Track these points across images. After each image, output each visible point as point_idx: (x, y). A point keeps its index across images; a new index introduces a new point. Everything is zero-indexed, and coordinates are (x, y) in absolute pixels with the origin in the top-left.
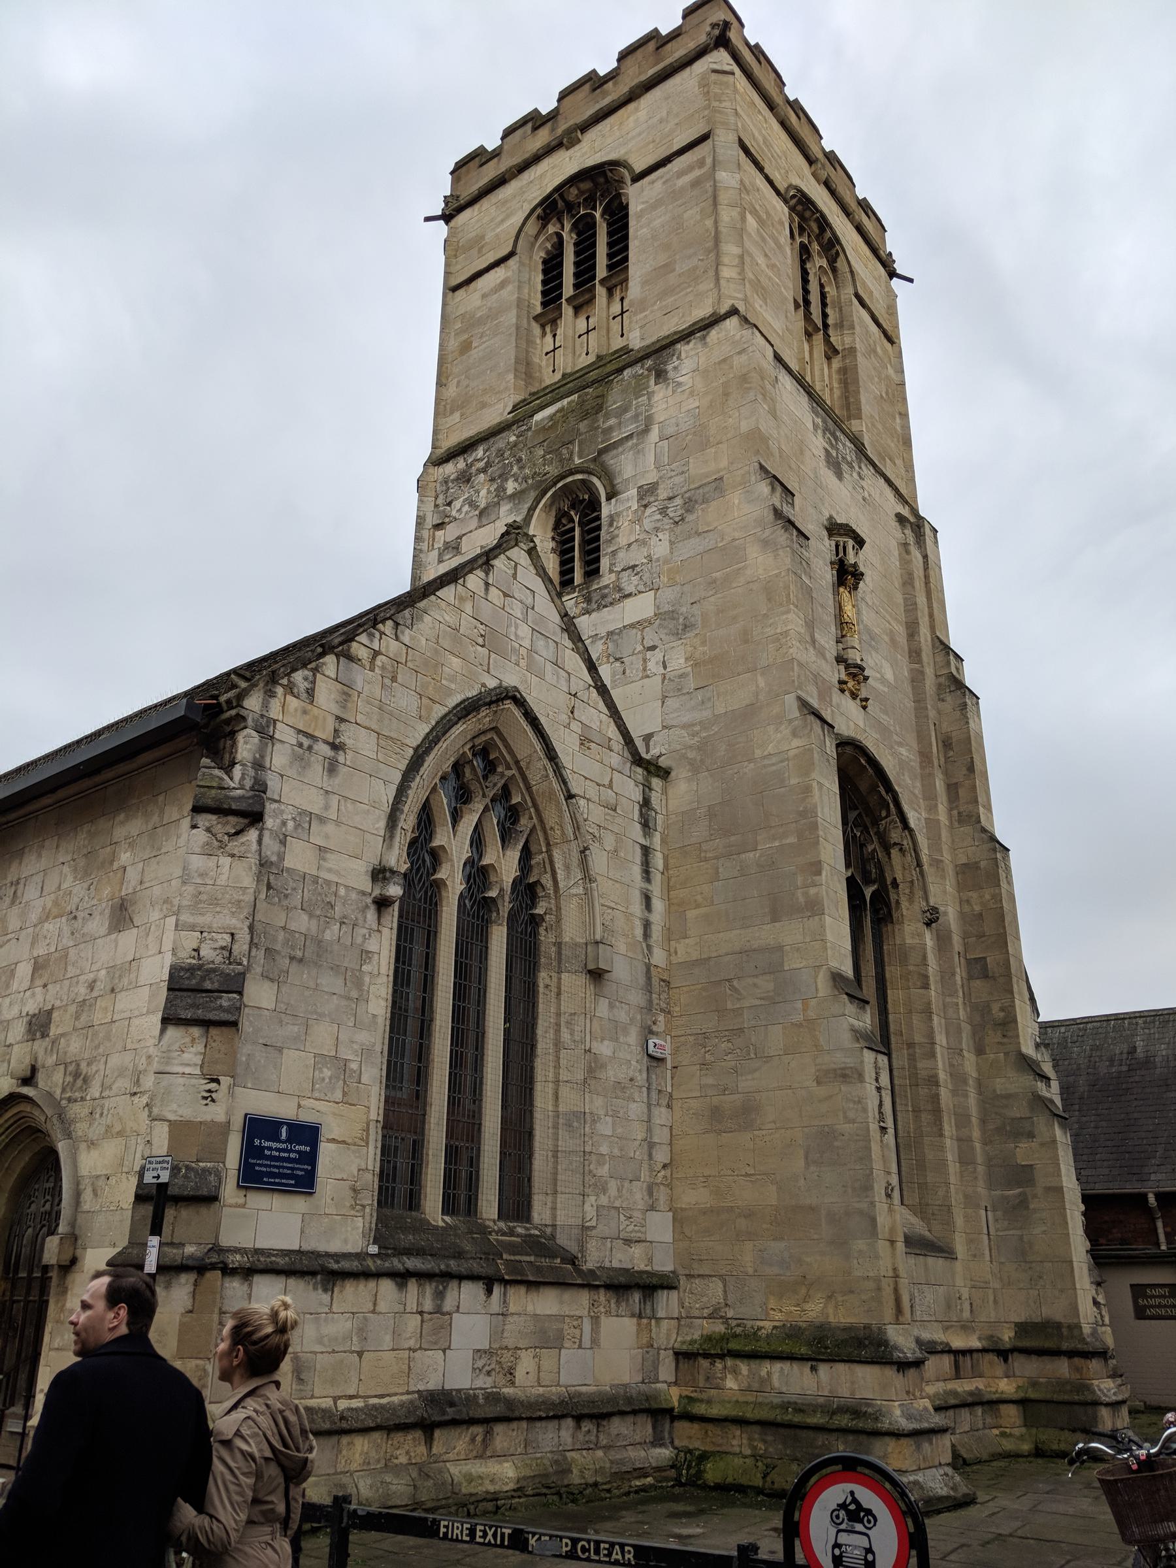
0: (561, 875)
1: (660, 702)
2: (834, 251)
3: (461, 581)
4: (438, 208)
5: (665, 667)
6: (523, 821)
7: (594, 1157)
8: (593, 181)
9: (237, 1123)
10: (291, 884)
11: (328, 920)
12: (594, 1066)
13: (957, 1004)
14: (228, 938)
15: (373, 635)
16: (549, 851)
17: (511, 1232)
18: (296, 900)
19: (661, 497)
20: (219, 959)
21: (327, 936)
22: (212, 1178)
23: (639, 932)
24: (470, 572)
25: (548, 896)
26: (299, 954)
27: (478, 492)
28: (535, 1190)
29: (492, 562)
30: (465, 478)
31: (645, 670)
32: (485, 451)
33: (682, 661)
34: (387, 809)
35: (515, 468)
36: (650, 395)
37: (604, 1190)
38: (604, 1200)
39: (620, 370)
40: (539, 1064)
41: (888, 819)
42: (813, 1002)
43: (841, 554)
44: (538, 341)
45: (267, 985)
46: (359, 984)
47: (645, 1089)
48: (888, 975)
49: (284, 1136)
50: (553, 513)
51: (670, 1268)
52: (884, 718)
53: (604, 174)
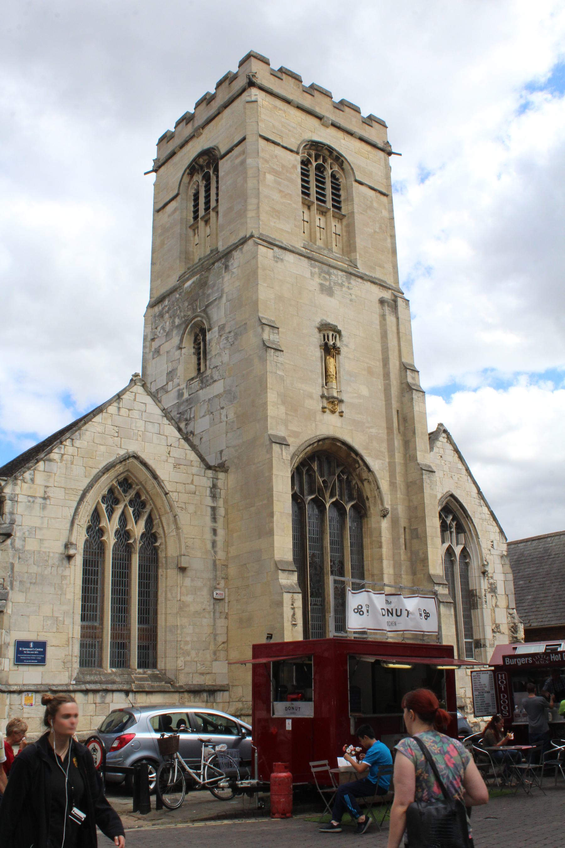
0: (166, 528)
1: (225, 435)
2: (340, 161)
3: (105, 411)
4: (150, 166)
5: (227, 418)
6: (148, 506)
7: (182, 643)
9: (12, 643)
10: (29, 556)
13: (400, 553)
14: (2, 580)
15: (61, 448)
16: (160, 518)
17: (144, 673)
21: (46, 573)
23: (209, 546)
24: (110, 405)
25: (161, 537)
26: (34, 581)
29: (122, 397)
30: (161, 315)
33: (233, 414)
34: (71, 518)
35: (178, 312)
36: (223, 278)
38: (188, 659)
40: (159, 607)
41: (360, 468)
43: (326, 340)
44: (192, 239)
50: (193, 335)
51: (227, 683)
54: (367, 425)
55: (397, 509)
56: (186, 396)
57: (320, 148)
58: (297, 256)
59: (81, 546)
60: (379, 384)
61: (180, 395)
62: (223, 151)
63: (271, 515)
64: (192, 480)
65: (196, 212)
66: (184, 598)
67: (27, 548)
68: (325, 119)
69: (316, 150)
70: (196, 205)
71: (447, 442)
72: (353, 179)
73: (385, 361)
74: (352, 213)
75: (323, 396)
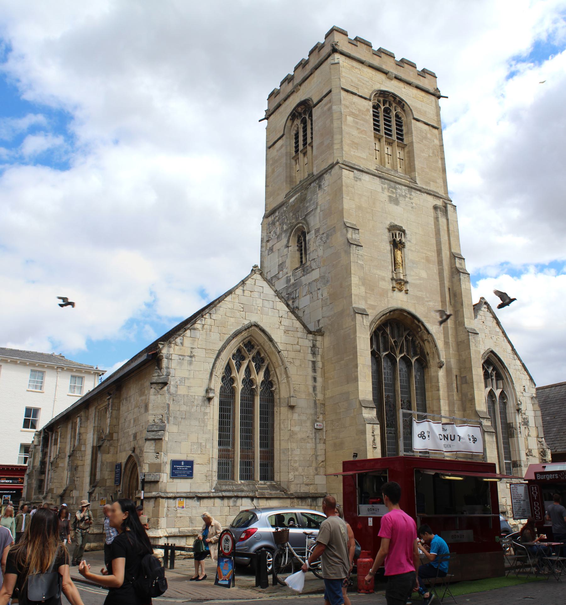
2: (402, 104)
3: (233, 293)
4: (263, 115)
6: (266, 361)
8: (305, 105)
9: (169, 462)
11: (193, 406)
12: (292, 434)
13: (453, 395)
14: (161, 416)
16: (275, 370)
17: (265, 484)
18: (182, 402)
19: (321, 233)
20: (159, 422)
21: (193, 411)
22: (158, 476)
23: (311, 390)
25: (276, 384)
27: (277, 229)
28: (275, 471)
29: (245, 283)
30: (273, 223)
31: (318, 297)
32: (278, 213)
33: (326, 294)
34: (210, 371)
36: (317, 194)
37: (297, 470)
38: (297, 473)
39: (310, 184)
40: (275, 435)
42: (356, 410)
43: (394, 237)
44: (294, 167)
45: (175, 426)
46: (204, 421)
47: (314, 439)
48: (426, 387)
49: (183, 464)
50: (297, 237)
52: (419, 294)
53: (306, 103)
54: (426, 299)
55: (450, 362)
56: (292, 281)
57: (386, 96)
58: (371, 176)
59: (218, 390)
60: (435, 269)
61: (288, 281)
62: (315, 101)
63: (356, 366)
64: (298, 342)
65: (297, 147)
66: (293, 429)
67: (179, 393)
68: (390, 74)
69: (384, 97)
70: (297, 142)
71: (488, 311)
72: (412, 117)
73: (439, 252)
74: (412, 143)
75: (392, 279)
